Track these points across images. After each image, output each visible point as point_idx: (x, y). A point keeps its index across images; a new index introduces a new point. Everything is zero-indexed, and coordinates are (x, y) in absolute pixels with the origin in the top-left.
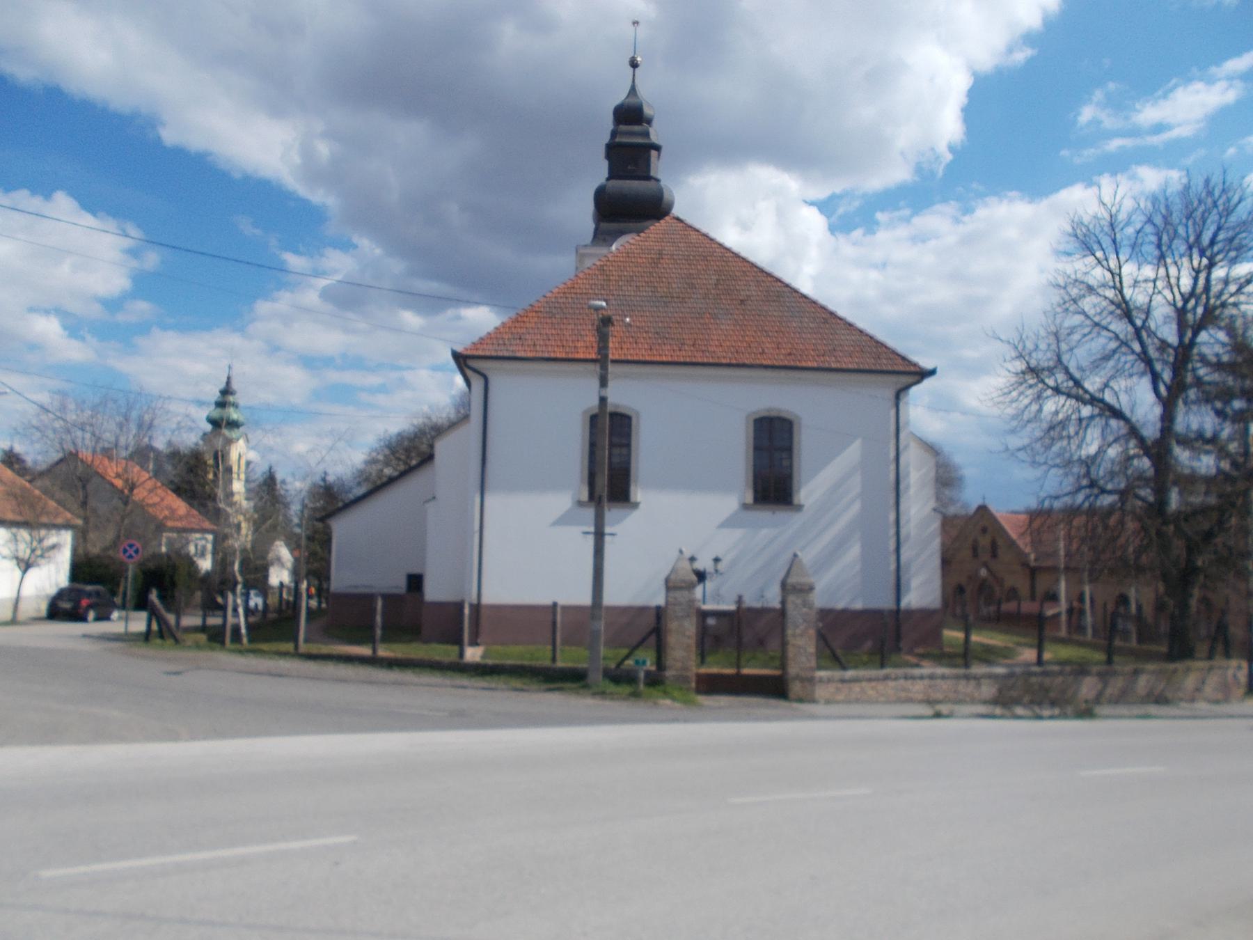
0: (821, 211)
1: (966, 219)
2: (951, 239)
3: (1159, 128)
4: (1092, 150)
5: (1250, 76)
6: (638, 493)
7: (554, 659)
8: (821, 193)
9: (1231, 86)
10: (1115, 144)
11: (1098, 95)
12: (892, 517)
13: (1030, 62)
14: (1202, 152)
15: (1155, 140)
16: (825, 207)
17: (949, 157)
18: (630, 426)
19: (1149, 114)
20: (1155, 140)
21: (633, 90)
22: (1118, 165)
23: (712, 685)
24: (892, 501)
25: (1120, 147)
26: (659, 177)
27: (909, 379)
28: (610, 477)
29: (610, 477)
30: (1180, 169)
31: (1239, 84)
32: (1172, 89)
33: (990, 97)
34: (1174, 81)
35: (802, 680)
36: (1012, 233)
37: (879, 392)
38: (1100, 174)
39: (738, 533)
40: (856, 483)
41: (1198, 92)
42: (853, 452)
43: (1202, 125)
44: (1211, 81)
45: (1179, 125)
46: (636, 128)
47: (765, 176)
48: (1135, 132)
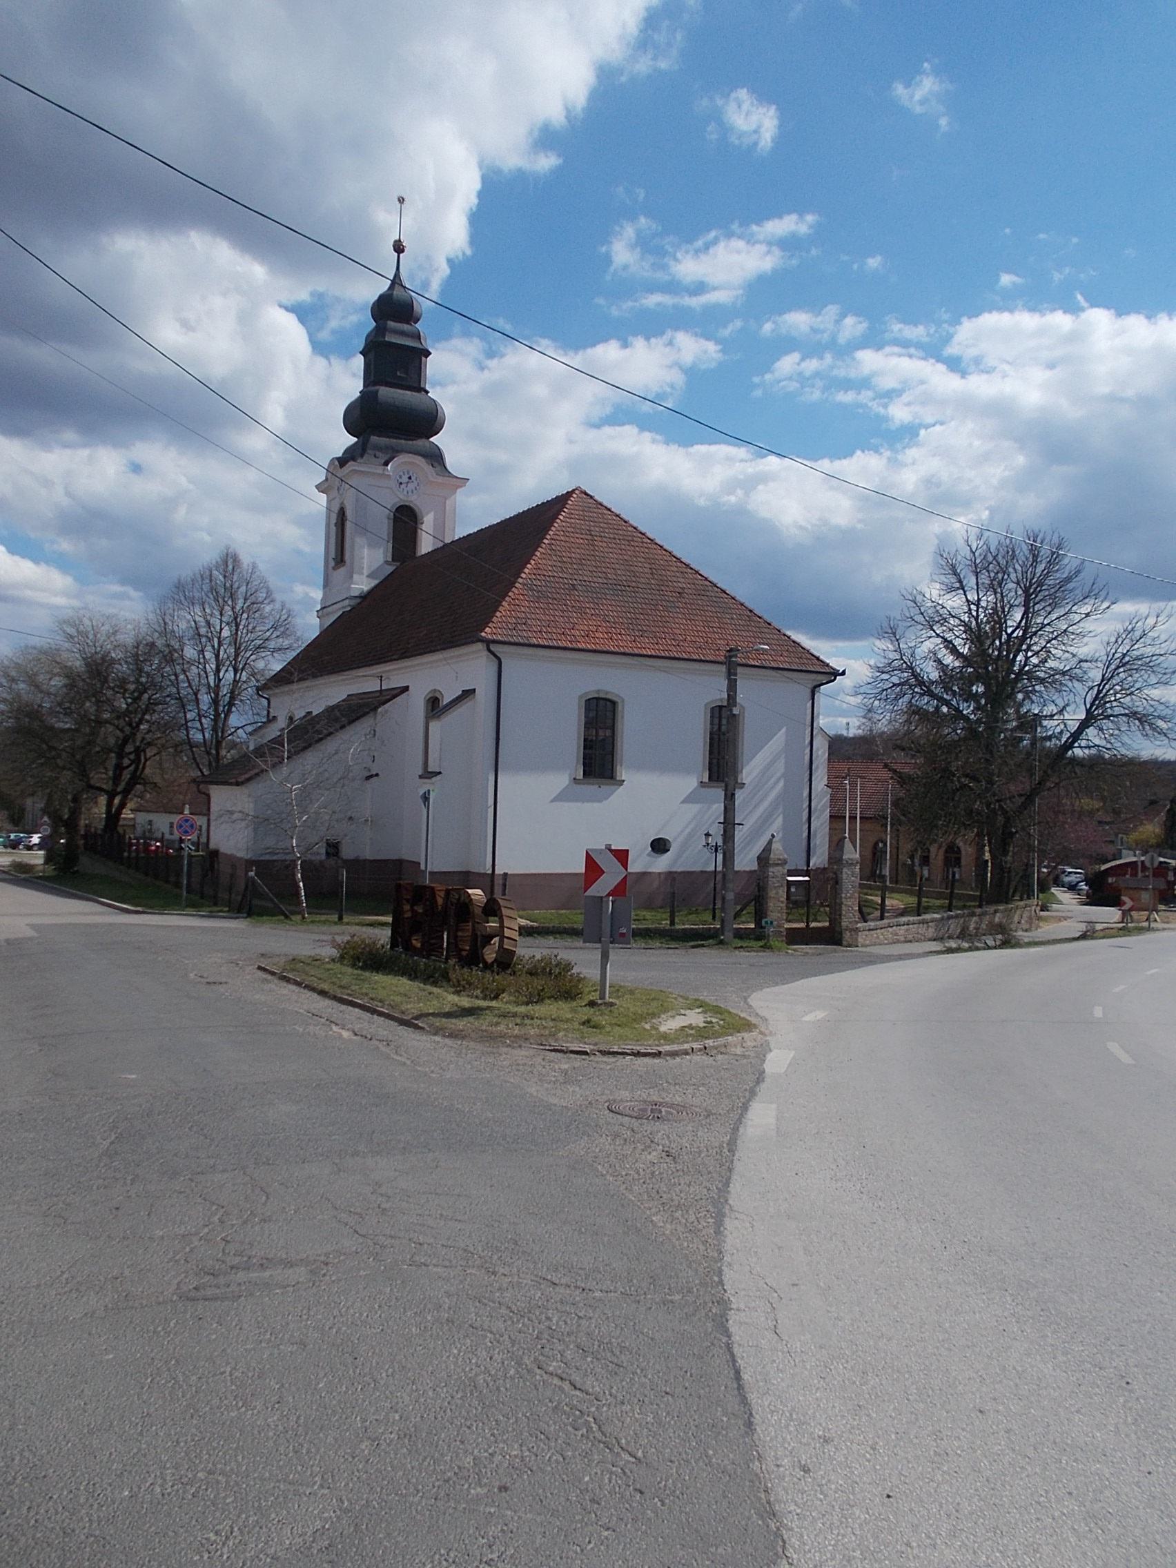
0: (302, 320)
1: (493, 363)
2: (474, 387)
3: (700, 288)
4: (630, 304)
5: (788, 244)
6: (623, 773)
7: (672, 923)
8: (303, 295)
9: (769, 252)
10: (653, 300)
11: (629, 231)
12: (806, 793)
13: (557, 172)
14: (738, 323)
15: (694, 302)
16: (302, 312)
17: (445, 270)
18: (614, 712)
19: (688, 268)
20: (694, 302)
21: (396, 281)
22: (651, 326)
23: (794, 937)
24: (807, 779)
25: (659, 304)
26: (427, 388)
27: (824, 678)
28: (599, 761)
29: (599, 761)
30: (717, 342)
31: (776, 251)
32: (715, 242)
33: (500, 198)
34: (713, 234)
35: (851, 930)
36: (540, 390)
37: (797, 689)
38: (635, 335)
39: (694, 808)
40: (780, 767)
41: (738, 252)
42: (780, 737)
43: (741, 292)
44: (751, 241)
45: (715, 289)
46: (405, 327)
47: (221, 254)
48: (673, 287)
